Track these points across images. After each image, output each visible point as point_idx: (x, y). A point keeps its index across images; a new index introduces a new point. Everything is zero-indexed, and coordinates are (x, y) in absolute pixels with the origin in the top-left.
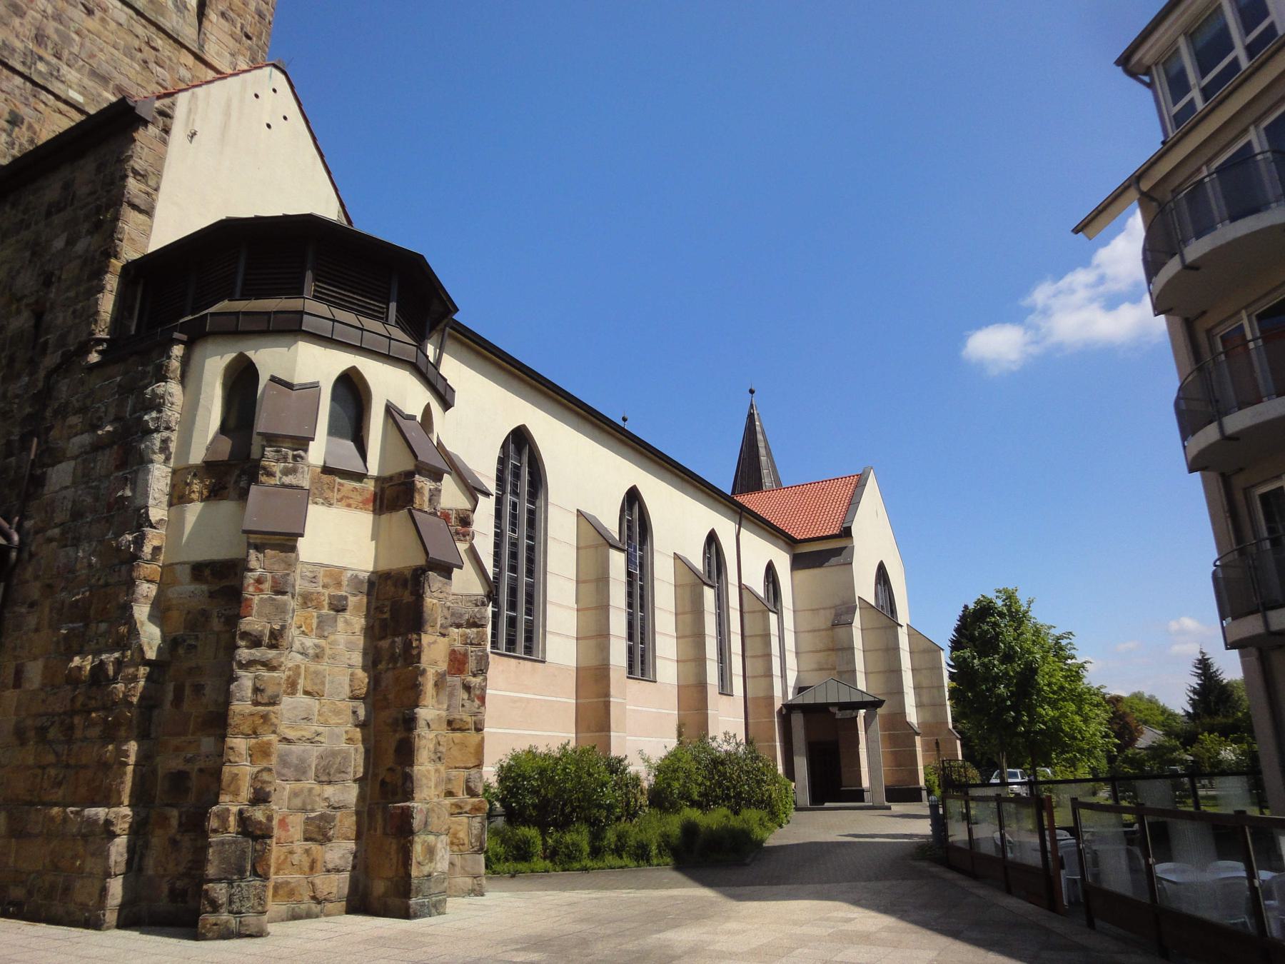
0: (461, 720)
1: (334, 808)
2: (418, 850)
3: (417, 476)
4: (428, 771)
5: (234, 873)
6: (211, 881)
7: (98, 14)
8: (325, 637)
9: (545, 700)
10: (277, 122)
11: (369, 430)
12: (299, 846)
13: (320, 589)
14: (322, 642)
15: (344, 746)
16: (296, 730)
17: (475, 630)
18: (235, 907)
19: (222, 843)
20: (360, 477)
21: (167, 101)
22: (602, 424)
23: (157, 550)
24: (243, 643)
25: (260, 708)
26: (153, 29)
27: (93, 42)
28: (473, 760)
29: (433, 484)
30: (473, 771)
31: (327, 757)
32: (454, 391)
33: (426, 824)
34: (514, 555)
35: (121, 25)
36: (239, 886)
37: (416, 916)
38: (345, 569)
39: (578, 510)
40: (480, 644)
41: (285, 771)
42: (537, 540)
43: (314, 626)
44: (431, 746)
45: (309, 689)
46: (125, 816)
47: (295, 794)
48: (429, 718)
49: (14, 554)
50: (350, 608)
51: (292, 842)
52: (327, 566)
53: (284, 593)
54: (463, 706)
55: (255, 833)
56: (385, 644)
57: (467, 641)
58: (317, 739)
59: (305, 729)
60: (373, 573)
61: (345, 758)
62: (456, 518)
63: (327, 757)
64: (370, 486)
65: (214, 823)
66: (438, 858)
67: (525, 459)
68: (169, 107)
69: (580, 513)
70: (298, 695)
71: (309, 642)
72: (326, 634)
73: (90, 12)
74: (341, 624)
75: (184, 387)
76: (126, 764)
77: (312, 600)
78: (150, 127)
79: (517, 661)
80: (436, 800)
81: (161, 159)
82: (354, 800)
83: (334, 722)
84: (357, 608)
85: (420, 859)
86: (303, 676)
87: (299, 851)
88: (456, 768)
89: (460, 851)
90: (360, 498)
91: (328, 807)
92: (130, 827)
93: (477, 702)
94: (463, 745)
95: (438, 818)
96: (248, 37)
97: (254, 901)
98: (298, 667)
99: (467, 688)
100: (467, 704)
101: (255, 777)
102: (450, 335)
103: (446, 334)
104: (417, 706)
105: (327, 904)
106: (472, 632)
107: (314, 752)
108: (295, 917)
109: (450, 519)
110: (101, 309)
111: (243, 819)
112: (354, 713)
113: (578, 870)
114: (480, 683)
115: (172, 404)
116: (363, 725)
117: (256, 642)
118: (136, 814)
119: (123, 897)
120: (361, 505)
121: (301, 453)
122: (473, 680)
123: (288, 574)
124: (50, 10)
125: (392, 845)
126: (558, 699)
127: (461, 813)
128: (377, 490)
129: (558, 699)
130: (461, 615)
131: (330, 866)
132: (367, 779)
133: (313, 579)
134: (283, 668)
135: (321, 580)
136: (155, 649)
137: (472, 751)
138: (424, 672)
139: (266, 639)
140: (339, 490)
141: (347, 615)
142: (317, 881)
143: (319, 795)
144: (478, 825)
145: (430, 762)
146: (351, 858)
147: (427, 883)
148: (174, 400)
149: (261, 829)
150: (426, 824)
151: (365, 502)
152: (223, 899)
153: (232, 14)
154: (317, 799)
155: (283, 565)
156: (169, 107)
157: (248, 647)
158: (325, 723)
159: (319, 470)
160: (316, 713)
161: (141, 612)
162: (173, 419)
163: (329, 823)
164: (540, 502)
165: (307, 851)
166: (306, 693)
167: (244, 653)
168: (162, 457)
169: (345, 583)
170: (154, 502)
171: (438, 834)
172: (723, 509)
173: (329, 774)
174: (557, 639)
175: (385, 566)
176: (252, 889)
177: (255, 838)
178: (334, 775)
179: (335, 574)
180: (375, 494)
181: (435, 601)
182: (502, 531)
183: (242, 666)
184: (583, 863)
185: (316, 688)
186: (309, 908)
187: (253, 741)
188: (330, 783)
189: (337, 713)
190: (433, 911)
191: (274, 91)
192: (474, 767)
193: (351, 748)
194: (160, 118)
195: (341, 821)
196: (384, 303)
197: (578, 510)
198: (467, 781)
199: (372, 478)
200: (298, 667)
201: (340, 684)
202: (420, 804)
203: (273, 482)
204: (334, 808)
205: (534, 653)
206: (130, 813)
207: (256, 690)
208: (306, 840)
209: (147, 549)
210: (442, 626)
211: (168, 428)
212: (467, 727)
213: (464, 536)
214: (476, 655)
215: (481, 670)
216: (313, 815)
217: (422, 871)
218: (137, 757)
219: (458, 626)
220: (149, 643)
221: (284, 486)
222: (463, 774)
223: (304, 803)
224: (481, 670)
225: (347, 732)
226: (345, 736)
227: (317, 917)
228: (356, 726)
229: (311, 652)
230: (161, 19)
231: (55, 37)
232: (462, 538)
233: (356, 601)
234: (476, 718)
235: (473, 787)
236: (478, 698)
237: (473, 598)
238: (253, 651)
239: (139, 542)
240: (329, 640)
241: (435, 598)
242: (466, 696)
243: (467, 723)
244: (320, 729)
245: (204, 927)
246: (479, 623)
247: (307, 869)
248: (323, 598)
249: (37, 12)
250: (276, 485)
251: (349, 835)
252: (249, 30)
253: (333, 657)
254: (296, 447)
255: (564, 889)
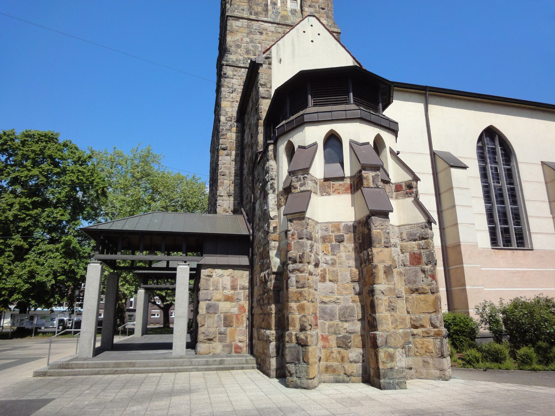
0: (423, 288)
1: (350, 333)
2: (382, 355)
3: (363, 171)
4: (386, 316)
5: (296, 360)
6: (288, 363)
7: (264, 32)
8: (336, 255)
9: (537, 271)
10: (316, 39)
11: (512, 147)
12: (335, 350)
13: (330, 233)
14: (334, 257)
15: (351, 304)
16: (328, 298)
17: (424, 241)
18: (298, 375)
19: (290, 347)
20: (342, 178)
21: (268, 52)
22: (548, 109)
23: (275, 228)
24: (290, 262)
25: (299, 289)
26: (285, 27)
27: (265, 43)
28: (432, 309)
29: (374, 173)
30: (433, 315)
31: (343, 309)
32: (397, 123)
33: (386, 342)
34: (501, 195)
35: (273, 32)
36: (298, 366)
37: (384, 388)
38: (341, 222)
39: (542, 162)
40: (427, 248)
41: (325, 316)
42: (515, 184)
43: (330, 251)
44: (387, 303)
45: (331, 279)
46: (273, 334)
47: (330, 326)
48: (382, 289)
49: (251, 237)
50: (346, 240)
51: (332, 348)
52: (332, 222)
53: (302, 238)
54: (423, 281)
55: (303, 344)
56: (362, 255)
57: (420, 248)
58: (338, 301)
59: (331, 297)
60: (355, 222)
61: (352, 310)
62: (405, 186)
63: (343, 309)
64: (348, 181)
65: (287, 339)
66: (397, 360)
67: (497, 142)
68: (269, 54)
69: (543, 163)
70: (327, 282)
71: (328, 258)
72: (336, 253)
73: (261, 33)
74: (342, 248)
75: (276, 161)
76: (272, 314)
77: (327, 239)
78: (264, 65)
79: (512, 251)
80: (393, 330)
81: (270, 75)
82: (359, 330)
83: (345, 293)
84: (349, 239)
85: (384, 360)
86: (328, 273)
87: (335, 352)
88: (423, 313)
89: (431, 356)
90: (343, 188)
91: (347, 332)
92: (276, 338)
93: (430, 279)
94: (426, 301)
95: (395, 340)
96: (323, 9)
97: (304, 374)
98: (325, 269)
99: (423, 271)
100: (425, 279)
101: (300, 320)
102: (429, 94)
103: (427, 95)
104: (374, 284)
105: (352, 377)
106: (422, 242)
107: (337, 307)
108: (337, 381)
109: (402, 187)
110: (259, 141)
111: (297, 338)
112: (354, 288)
113: (529, 370)
114: (430, 268)
115: (272, 169)
116: (359, 294)
117: (295, 262)
118: (277, 333)
119: (277, 365)
120: (344, 192)
121: (306, 175)
122: (426, 267)
123: (303, 230)
124: (248, 40)
125: (372, 351)
126: (548, 269)
127: (429, 336)
128: (352, 183)
129: (548, 269)
130: (415, 235)
131: (351, 360)
132: (365, 320)
133: (327, 230)
134: (306, 271)
135: (330, 229)
136: (277, 267)
137: (431, 304)
138: (376, 267)
139: (298, 260)
140: (333, 187)
141: (345, 243)
142: (346, 366)
143: (342, 327)
144: (439, 343)
145: (386, 311)
146: (361, 357)
147: (390, 373)
148: (273, 167)
149: (303, 342)
150: (386, 342)
151: (346, 190)
152: (293, 371)
153: (313, 4)
154: (341, 329)
155: (301, 227)
156: (269, 54)
157: (292, 264)
158: (341, 294)
159: (323, 180)
160: (336, 290)
161: (273, 253)
162: (274, 175)
163: (348, 340)
164: (513, 163)
165: (339, 352)
166: (330, 281)
167: (291, 267)
168: (272, 191)
169: (342, 229)
170: (271, 209)
171: (395, 348)
172: (414, 96)
173: (345, 317)
174: (539, 236)
175: (358, 219)
176: (303, 368)
177: (302, 346)
178: (348, 318)
179: (336, 226)
180: (351, 185)
181: (378, 231)
182: (489, 184)
183: (291, 272)
184: (533, 366)
185: (334, 278)
186: (344, 378)
187: (298, 304)
188: (346, 321)
189: (346, 289)
190: (397, 387)
191: (312, 26)
192: (433, 312)
193: (355, 305)
194: (266, 60)
195: (354, 339)
196: (346, 95)
197: (542, 162)
198: (430, 320)
199: (348, 177)
200: (325, 269)
201: (345, 275)
202: (381, 333)
203: (297, 191)
204: (350, 333)
205: (526, 244)
206: (275, 333)
207: (297, 282)
208: (338, 347)
209: (271, 228)
210: (385, 242)
211: (272, 179)
212: (426, 292)
213: (411, 194)
214: (426, 254)
215: (429, 261)
216: (340, 336)
217: (386, 366)
218: (276, 310)
219: (415, 240)
220: (274, 265)
221: (302, 192)
222: (429, 316)
223: (335, 331)
224: (429, 261)
225: (351, 298)
226: (351, 300)
227: (348, 382)
228: (356, 294)
229: (330, 262)
230: (287, 21)
231: (252, 49)
232: (410, 195)
233: (348, 236)
234: (430, 287)
235: (434, 323)
236: (430, 276)
237: (420, 225)
238: (294, 265)
239: (268, 227)
240: (337, 256)
241: (379, 229)
242: (423, 276)
243: (426, 290)
244: (339, 297)
245: (288, 382)
246: (425, 237)
247: (340, 360)
248: (332, 237)
249: (245, 43)
250: (298, 192)
251: (359, 345)
252: (323, 6)
253: (340, 263)
254: (304, 173)
255: (499, 382)
